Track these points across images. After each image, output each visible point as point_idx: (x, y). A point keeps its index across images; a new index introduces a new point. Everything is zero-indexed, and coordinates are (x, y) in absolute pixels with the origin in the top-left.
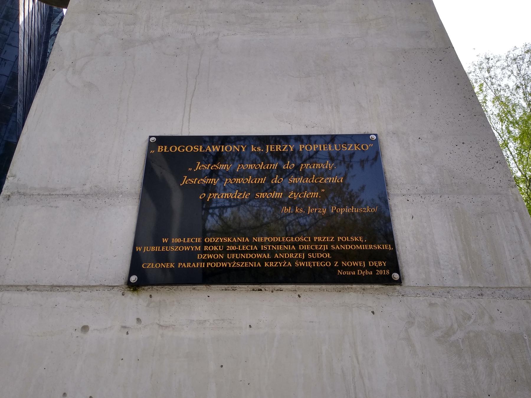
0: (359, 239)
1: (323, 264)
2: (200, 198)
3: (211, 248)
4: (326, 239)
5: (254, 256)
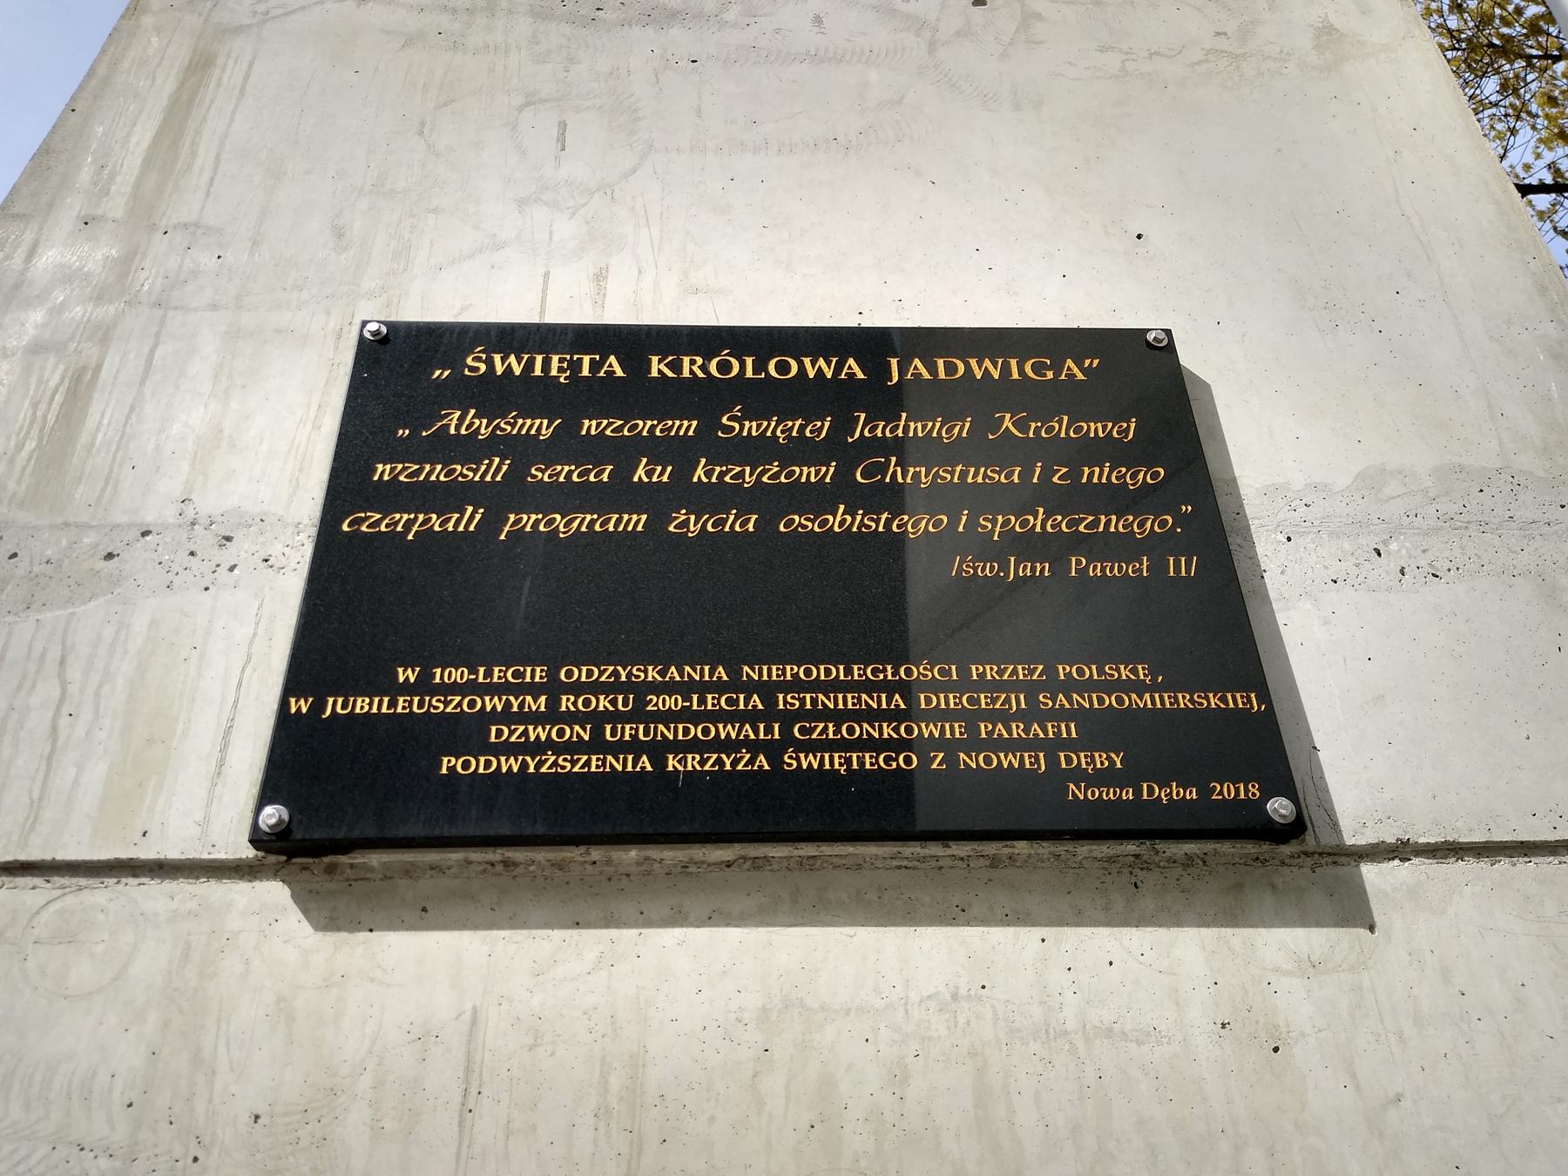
0: (1134, 671)
1: (887, 760)
3: (587, 703)
4: (1015, 672)
5: (706, 731)
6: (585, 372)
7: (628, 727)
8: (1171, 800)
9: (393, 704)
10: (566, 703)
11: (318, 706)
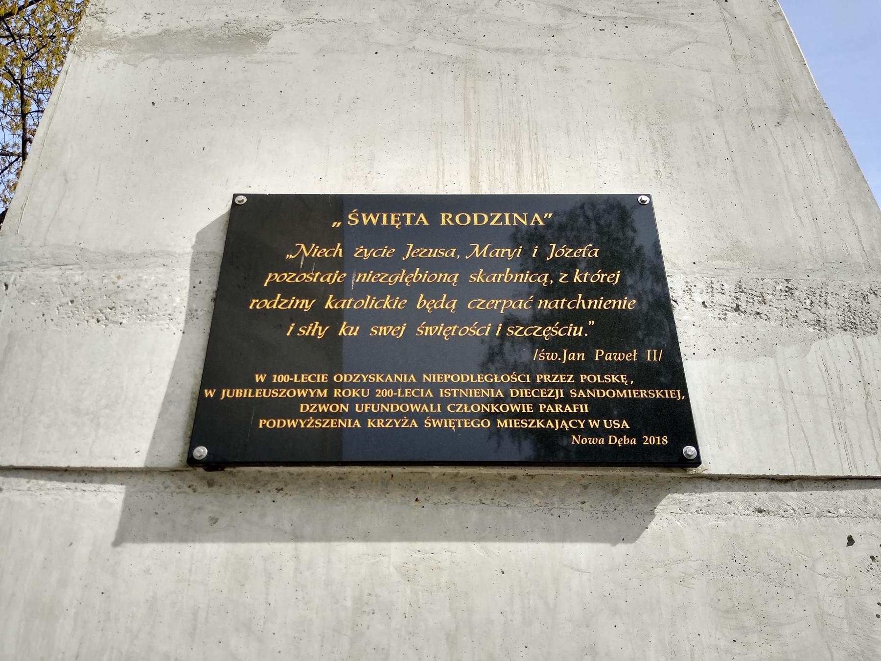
4: (559, 378)
6: (409, 222)
8: (623, 445)
9: (253, 393)
10: (336, 393)
11: (218, 394)
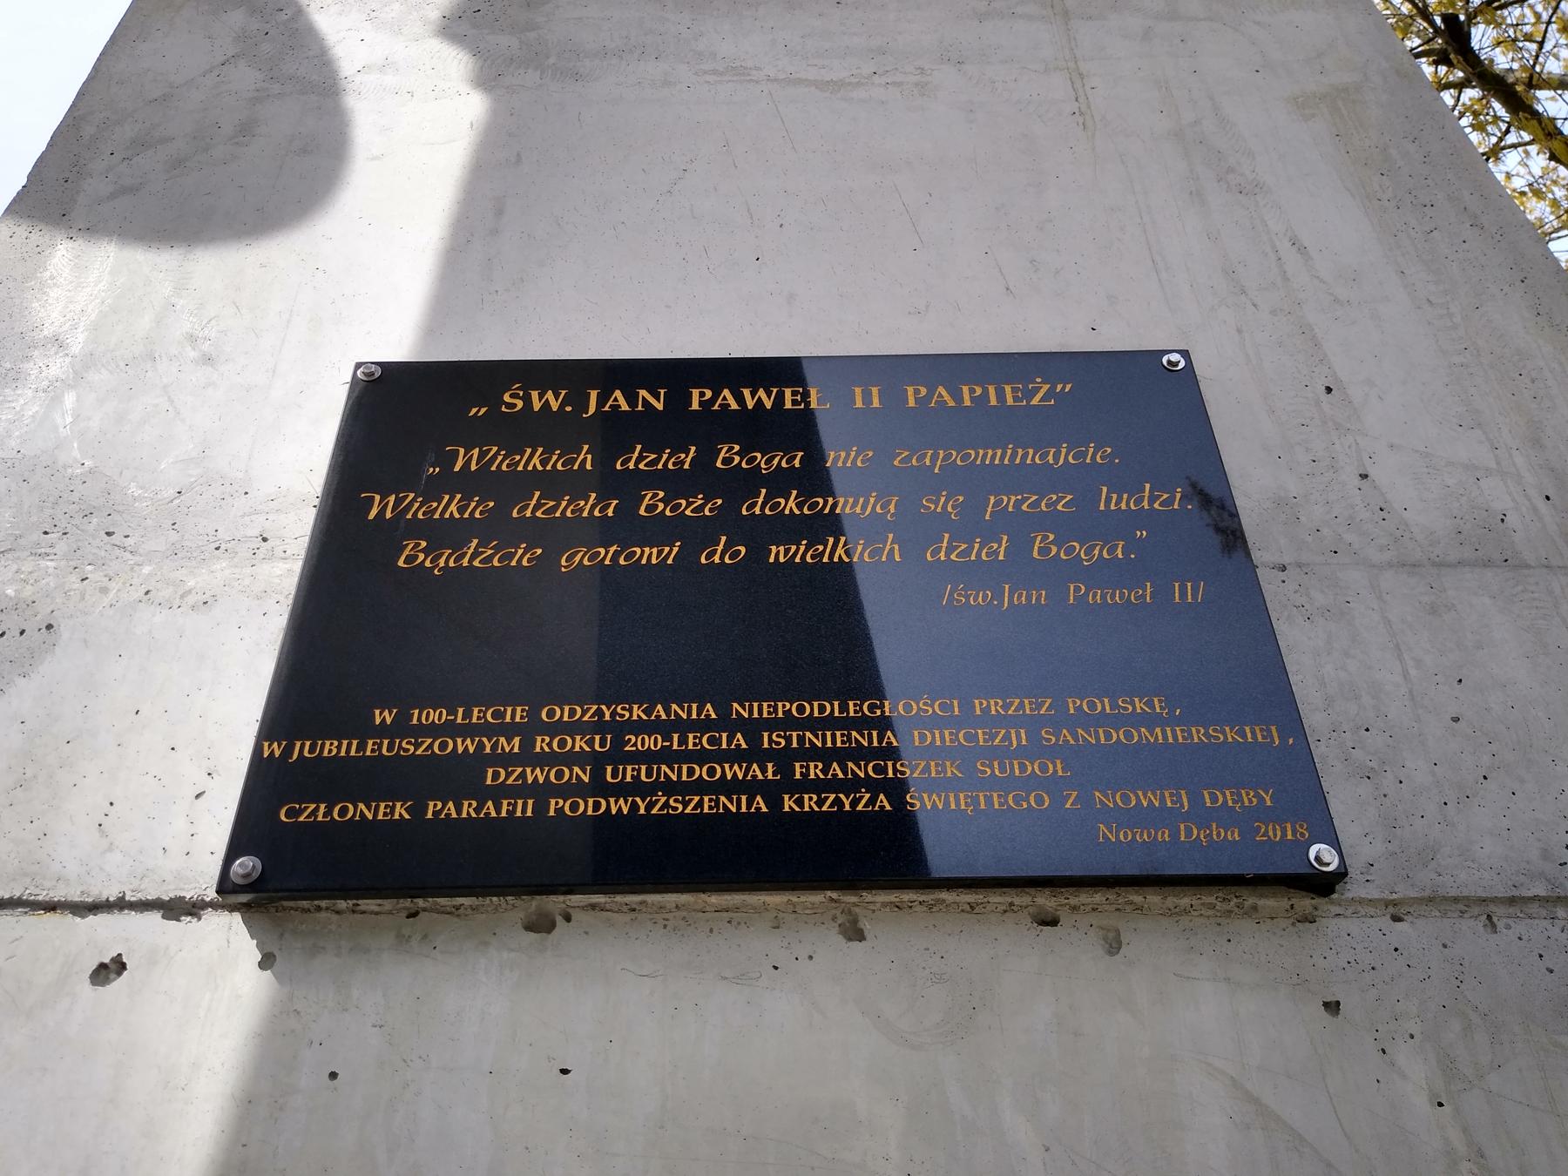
0: (1150, 704)
2: (703, 561)
3: (562, 744)
5: (711, 772)
7: (629, 768)
10: (541, 744)
